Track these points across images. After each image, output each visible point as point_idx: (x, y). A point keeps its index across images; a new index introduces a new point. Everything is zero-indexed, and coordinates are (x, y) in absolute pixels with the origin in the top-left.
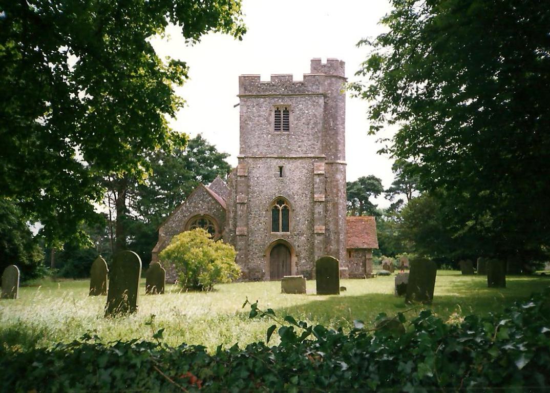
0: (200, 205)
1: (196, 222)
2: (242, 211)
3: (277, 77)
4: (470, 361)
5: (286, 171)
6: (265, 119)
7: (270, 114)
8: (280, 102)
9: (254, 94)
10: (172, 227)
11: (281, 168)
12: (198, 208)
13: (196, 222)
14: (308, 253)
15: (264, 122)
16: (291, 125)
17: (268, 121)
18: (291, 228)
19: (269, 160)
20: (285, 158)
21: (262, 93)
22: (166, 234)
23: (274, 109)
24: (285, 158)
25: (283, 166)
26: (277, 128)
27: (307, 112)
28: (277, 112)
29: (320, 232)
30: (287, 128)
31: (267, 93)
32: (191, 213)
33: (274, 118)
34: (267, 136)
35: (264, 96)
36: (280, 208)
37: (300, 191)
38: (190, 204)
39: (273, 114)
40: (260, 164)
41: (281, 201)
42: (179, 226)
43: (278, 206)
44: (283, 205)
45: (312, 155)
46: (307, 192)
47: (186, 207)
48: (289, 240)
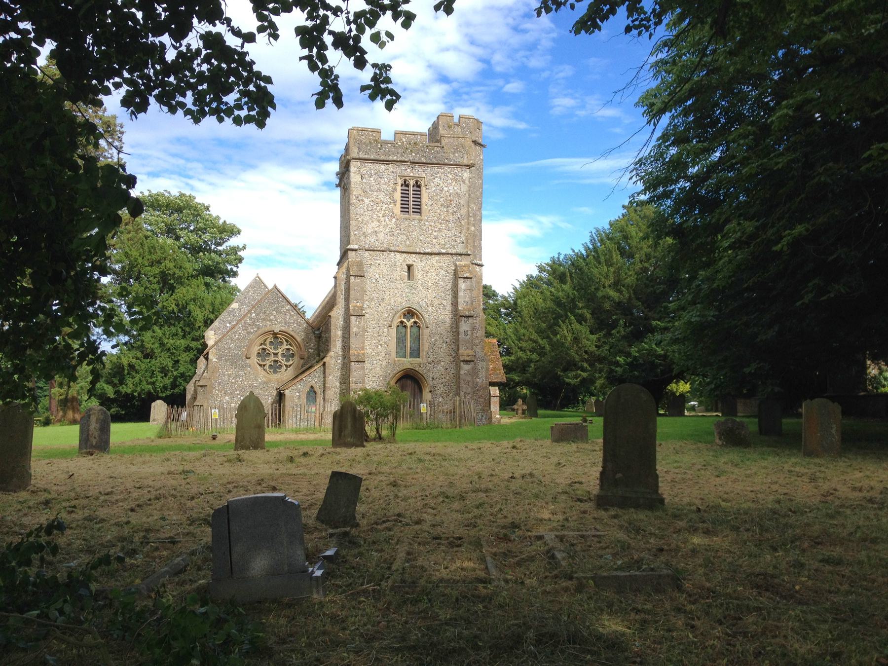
0: (272, 317)
1: (265, 340)
2: (358, 327)
3: (404, 133)
4: (166, 375)
5: (418, 274)
6: (386, 195)
7: (395, 190)
8: (409, 172)
9: (372, 157)
10: (230, 348)
11: (409, 267)
12: (271, 320)
13: (265, 340)
14: (445, 388)
15: (387, 199)
16: (425, 208)
17: (392, 198)
18: (423, 353)
19: (392, 254)
20: (416, 253)
21: (383, 158)
22: (220, 359)
23: (400, 182)
24: (416, 253)
25: (412, 265)
26: (405, 209)
27: (446, 189)
28: (406, 184)
29: (468, 359)
30: (418, 210)
31: (390, 158)
32: (259, 328)
33: (400, 195)
34: (390, 221)
35: (387, 162)
36: (409, 324)
37: (436, 302)
38: (257, 315)
39: (399, 188)
40: (381, 259)
41: (410, 313)
42: (240, 347)
43: (405, 320)
44: (412, 320)
45: (453, 251)
46: (445, 302)
47: (251, 319)
48: (421, 370)
